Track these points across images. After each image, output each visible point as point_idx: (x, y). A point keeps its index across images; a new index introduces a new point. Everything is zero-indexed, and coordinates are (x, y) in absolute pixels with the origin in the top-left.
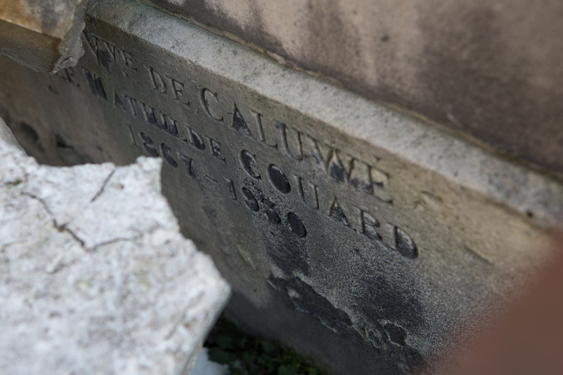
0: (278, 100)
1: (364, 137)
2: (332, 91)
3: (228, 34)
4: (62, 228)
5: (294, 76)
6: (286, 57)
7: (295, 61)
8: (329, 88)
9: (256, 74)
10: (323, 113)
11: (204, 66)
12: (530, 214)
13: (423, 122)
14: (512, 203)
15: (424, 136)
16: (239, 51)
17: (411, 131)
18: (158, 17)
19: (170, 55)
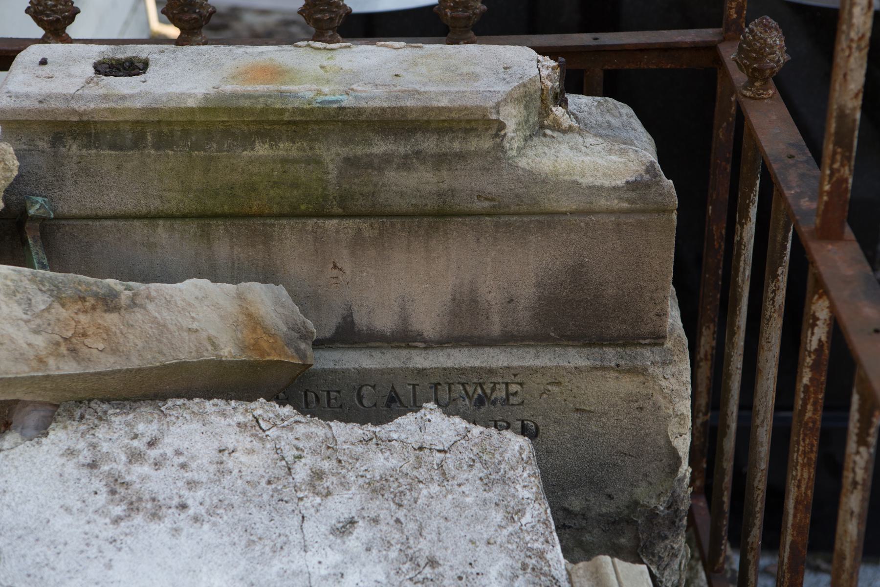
0: (436, 366)
1: (505, 364)
2: (465, 351)
3: (373, 344)
4: (421, 448)
5: (434, 351)
6: (425, 342)
7: (432, 342)
8: (462, 350)
9: (409, 359)
10: (471, 362)
11: (368, 367)
12: (618, 365)
13: (532, 346)
14: (606, 364)
15: (538, 352)
16: (385, 351)
17: (528, 353)
18: (418, 121)
19: (333, 371)
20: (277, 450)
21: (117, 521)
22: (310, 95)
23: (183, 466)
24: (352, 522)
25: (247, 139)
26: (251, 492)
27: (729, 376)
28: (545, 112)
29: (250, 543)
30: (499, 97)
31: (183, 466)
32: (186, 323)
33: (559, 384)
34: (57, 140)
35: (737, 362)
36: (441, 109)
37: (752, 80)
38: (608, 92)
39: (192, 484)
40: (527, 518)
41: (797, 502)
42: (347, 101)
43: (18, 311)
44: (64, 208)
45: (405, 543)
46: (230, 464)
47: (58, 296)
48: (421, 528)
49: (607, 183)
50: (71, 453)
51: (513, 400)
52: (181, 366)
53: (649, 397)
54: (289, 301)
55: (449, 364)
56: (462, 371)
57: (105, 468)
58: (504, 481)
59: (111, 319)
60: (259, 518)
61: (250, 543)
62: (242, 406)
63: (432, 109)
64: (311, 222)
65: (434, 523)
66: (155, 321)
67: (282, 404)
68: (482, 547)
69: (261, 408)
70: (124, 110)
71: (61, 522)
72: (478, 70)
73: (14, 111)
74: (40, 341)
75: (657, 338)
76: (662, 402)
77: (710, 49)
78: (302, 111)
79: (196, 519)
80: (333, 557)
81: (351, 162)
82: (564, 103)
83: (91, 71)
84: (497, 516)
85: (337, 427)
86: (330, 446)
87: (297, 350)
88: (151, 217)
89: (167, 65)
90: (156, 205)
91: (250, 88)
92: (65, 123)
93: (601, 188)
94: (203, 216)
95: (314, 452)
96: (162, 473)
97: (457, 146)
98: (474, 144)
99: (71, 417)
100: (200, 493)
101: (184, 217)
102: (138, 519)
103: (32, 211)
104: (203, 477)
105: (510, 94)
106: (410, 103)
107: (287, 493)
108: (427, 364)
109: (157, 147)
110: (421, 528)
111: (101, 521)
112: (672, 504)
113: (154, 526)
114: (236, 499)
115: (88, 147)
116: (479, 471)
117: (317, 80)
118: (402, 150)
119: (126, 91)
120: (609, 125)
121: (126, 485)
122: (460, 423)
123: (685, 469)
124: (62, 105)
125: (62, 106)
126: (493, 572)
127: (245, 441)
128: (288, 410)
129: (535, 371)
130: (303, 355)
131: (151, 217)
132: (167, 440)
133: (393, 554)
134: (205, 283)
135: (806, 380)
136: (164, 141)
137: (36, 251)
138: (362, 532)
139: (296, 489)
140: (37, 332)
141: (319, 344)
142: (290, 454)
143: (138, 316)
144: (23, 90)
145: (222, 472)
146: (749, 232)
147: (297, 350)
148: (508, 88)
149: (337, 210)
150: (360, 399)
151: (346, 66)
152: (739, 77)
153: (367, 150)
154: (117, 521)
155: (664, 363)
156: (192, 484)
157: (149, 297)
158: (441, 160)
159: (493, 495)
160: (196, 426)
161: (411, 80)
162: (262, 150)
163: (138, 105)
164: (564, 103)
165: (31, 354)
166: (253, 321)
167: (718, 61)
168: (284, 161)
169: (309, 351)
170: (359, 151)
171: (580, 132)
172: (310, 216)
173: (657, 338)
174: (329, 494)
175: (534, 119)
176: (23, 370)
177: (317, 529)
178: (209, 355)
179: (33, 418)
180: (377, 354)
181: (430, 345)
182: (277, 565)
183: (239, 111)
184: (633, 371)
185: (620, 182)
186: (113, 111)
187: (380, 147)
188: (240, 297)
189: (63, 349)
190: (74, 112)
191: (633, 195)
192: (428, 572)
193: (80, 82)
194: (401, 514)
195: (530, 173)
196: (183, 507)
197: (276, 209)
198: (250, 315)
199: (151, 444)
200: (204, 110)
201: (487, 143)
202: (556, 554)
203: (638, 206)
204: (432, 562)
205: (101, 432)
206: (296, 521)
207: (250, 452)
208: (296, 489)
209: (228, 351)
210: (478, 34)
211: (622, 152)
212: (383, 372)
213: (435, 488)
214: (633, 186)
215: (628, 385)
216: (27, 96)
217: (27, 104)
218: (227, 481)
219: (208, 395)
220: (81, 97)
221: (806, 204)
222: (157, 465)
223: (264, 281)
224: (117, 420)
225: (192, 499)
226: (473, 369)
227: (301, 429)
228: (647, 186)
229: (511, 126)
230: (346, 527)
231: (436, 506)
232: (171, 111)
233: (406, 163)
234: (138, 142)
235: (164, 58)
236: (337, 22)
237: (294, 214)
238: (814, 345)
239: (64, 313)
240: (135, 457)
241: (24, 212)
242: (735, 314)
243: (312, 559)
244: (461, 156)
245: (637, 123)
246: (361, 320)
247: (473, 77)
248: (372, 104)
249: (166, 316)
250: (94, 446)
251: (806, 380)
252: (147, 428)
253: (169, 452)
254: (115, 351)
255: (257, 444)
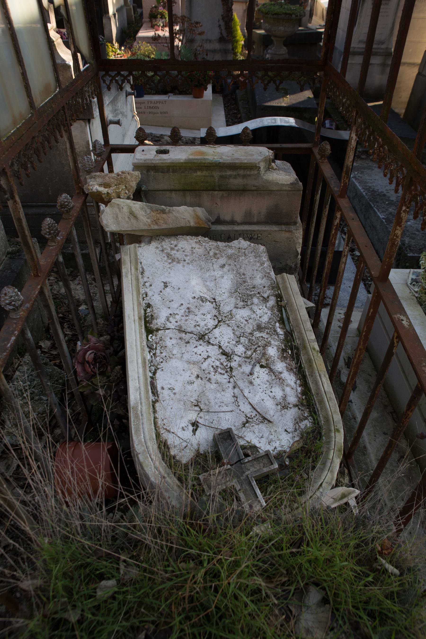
19: (215, 230)
20: (205, 248)
21: (170, 263)
22: (212, 159)
23: (184, 251)
24: (224, 265)
25: (195, 171)
26: (200, 258)
27: (310, 234)
28: (270, 164)
29: (201, 269)
30: (260, 160)
31: (184, 251)
32: (182, 217)
33: (270, 234)
34: (148, 171)
35: (313, 230)
36: (245, 163)
37: (322, 157)
38: (283, 160)
39: (186, 256)
40: (265, 265)
41: (328, 262)
42: (221, 161)
43: (144, 213)
44: (150, 188)
45: (237, 271)
46: (194, 251)
47: (152, 209)
48: (241, 267)
49: (285, 183)
50: (157, 248)
51: (259, 238)
52: (182, 227)
53: (292, 238)
54: (206, 212)
55: (244, 229)
56: (247, 231)
57: (166, 251)
58: (259, 256)
59: (164, 216)
60: (203, 263)
61: (201, 269)
62: (196, 238)
63: (242, 163)
64: (211, 192)
65: (244, 266)
66: (175, 216)
67: (205, 237)
68: (255, 271)
69: (200, 238)
70: (165, 163)
71: (157, 263)
72: (253, 153)
73: (138, 163)
74: (149, 221)
75: (295, 223)
76: (295, 239)
77: (310, 150)
78: (210, 163)
79: (188, 263)
80: (221, 273)
81: (221, 177)
82: (275, 162)
83: (155, 153)
84: (258, 265)
85: (219, 243)
86: (218, 247)
87: (208, 224)
88: (171, 190)
89: (174, 151)
90: (172, 187)
91: (196, 157)
92: (150, 166)
93: (284, 184)
94: (184, 190)
95: (214, 249)
96: (179, 253)
97: (248, 173)
98: (252, 172)
99: (156, 239)
100: (188, 258)
101: (179, 190)
102: (175, 263)
103: (143, 189)
104: (189, 254)
105: (262, 160)
106: (237, 161)
107: (209, 258)
108: (238, 229)
109: (173, 172)
110: (241, 267)
111: (167, 263)
112: (296, 265)
113: (178, 265)
114: (197, 259)
115: (156, 172)
116: (253, 254)
117: (213, 155)
118: (234, 174)
119: (165, 158)
120: (285, 169)
121: (171, 255)
122: (248, 243)
123: (299, 257)
124: (150, 162)
125: (150, 162)
126: (258, 277)
127: (197, 246)
128: (206, 239)
129: (265, 231)
130: (209, 226)
131: (171, 190)
132: (179, 245)
133: (235, 272)
134: (186, 207)
135: (333, 232)
136: (174, 171)
137: (144, 199)
138: (227, 267)
139: (211, 257)
140: (148, 218)
141: (213, 223)
142: (208, 249)
143: (171, 215)
144: (140, 158)
145: (193, 253)
146: (318, 197)
147: (208, 224)
148: (262, 158)
149: (217, 189)
150: (221, 237)
151: (220, 152)
152: (318, 157)
153: (226, 174)
154: (170, 263)
155: (296, 230)
156: (186, 256)
157: (173, 210)
158: (244, 176)
159: (257, 259)
160: (185, 242)
161: (237, 156)
162: (199, 173)
163: (169, 162)
164: (275, 162)
165: (147, 224)
166: (197, 217)
167: (312, 152)
168: (205, 176)
169: (211, 225)
170: (224, 174)
171: (278, 170)
172: (210, 190)
173: (295, 223)
174: (218, 258)
175: (267, 166)
176: (146, 228)
177: (216, 266)
178: (188, 225)
179: (147, 240)
180: (225, 226)
181: (239, 224)
182: (208, 274)
183: (194, 163)
184: (289, 231)
185: (289, 183)
186: (162, 163)
187: (229, 173)
188: (194, 211)
189: (154, 223)
190: (153, 163)
191: (291, 186)
192: (243, 276)
193: (153, 156)
194: (236, 263)
195: (266, 180)
196: (185, 261)
197: (202, 189)
198: (197, 215)
199: (176, 246)
200: (185, 163)
201: (256, 172)
202: (272, 273)
203: (293, 189)
204: (244, 274)
205: (163, 243)
206: (211, 264)
207: (199, 248)
208: (211, 257)
209: (192, 224)
210: (250, 143)
211: (289, 175)
212: (227, 231)
213: (243, 258)
214: (292, 184)
215: (288, 235)
216: (141, 159)
217: (141, 161)
218: (194, 255)
219: (187, 235)
220: (154, 160)
221: (336, 189)
222: (177, 251)
223: (199, 207)
224: (166, 240)
225: (187, 259)
226: (250, 230)
227: (210, 243)
228: (295, 184)
229: (262, 168)
230: (223, 266)
231: (244, 262)
232: (177, 163)
233: (235, 177)
234: (168, 171)
235: (173, 149)
236: (214, 140)
237: (207, 190)
238: (336, 224)
239: (154, 214)
240: (172, 249)
241: (141, 189)
242: (313, 218)
243: (216, 273)
244: (249, 175)
245: (291, 168)
246: (222, 217)
247: (253, 155)
248: (227, 162)
249: (177, 215)
250: (162, 246)
251: (333, 232)
252: (174, 242)
253: (180, 248)
254: (166, 223)
255: (200, 247)
